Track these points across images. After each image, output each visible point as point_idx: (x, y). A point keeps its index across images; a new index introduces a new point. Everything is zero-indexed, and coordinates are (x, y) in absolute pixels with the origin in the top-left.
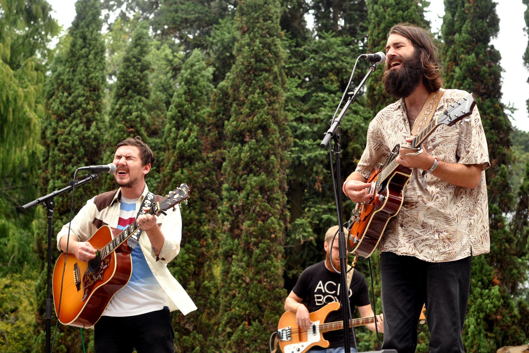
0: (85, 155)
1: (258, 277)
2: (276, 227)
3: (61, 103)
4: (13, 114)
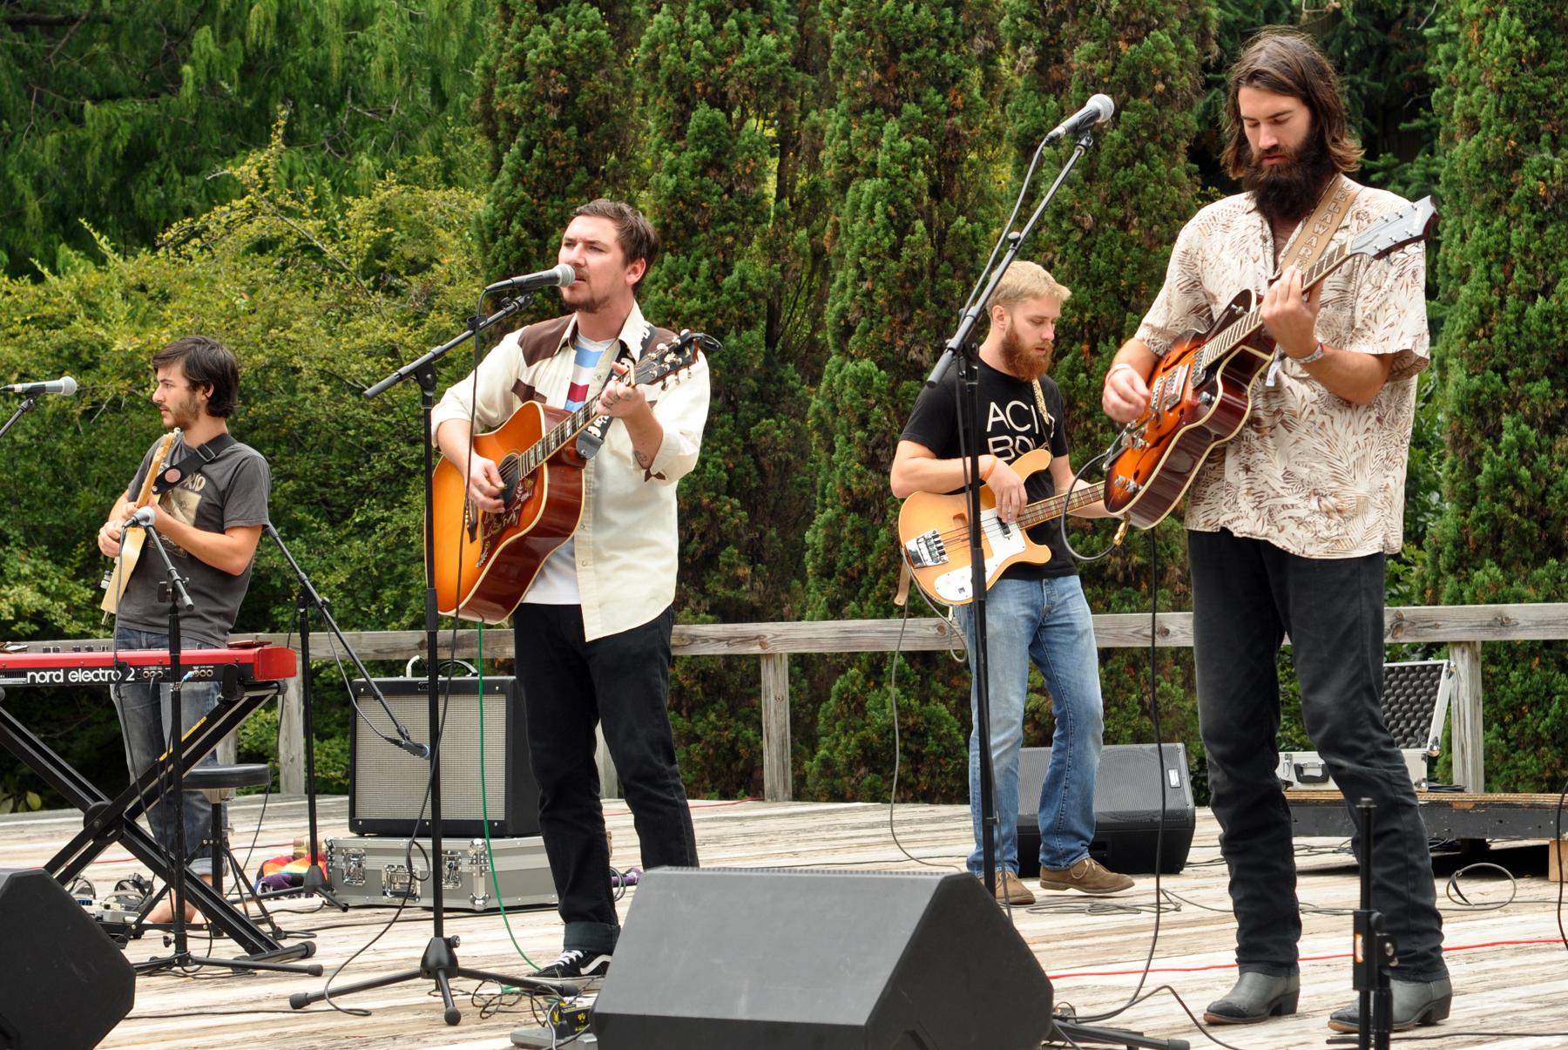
1: (1117, 212)
2: (1168, 61)
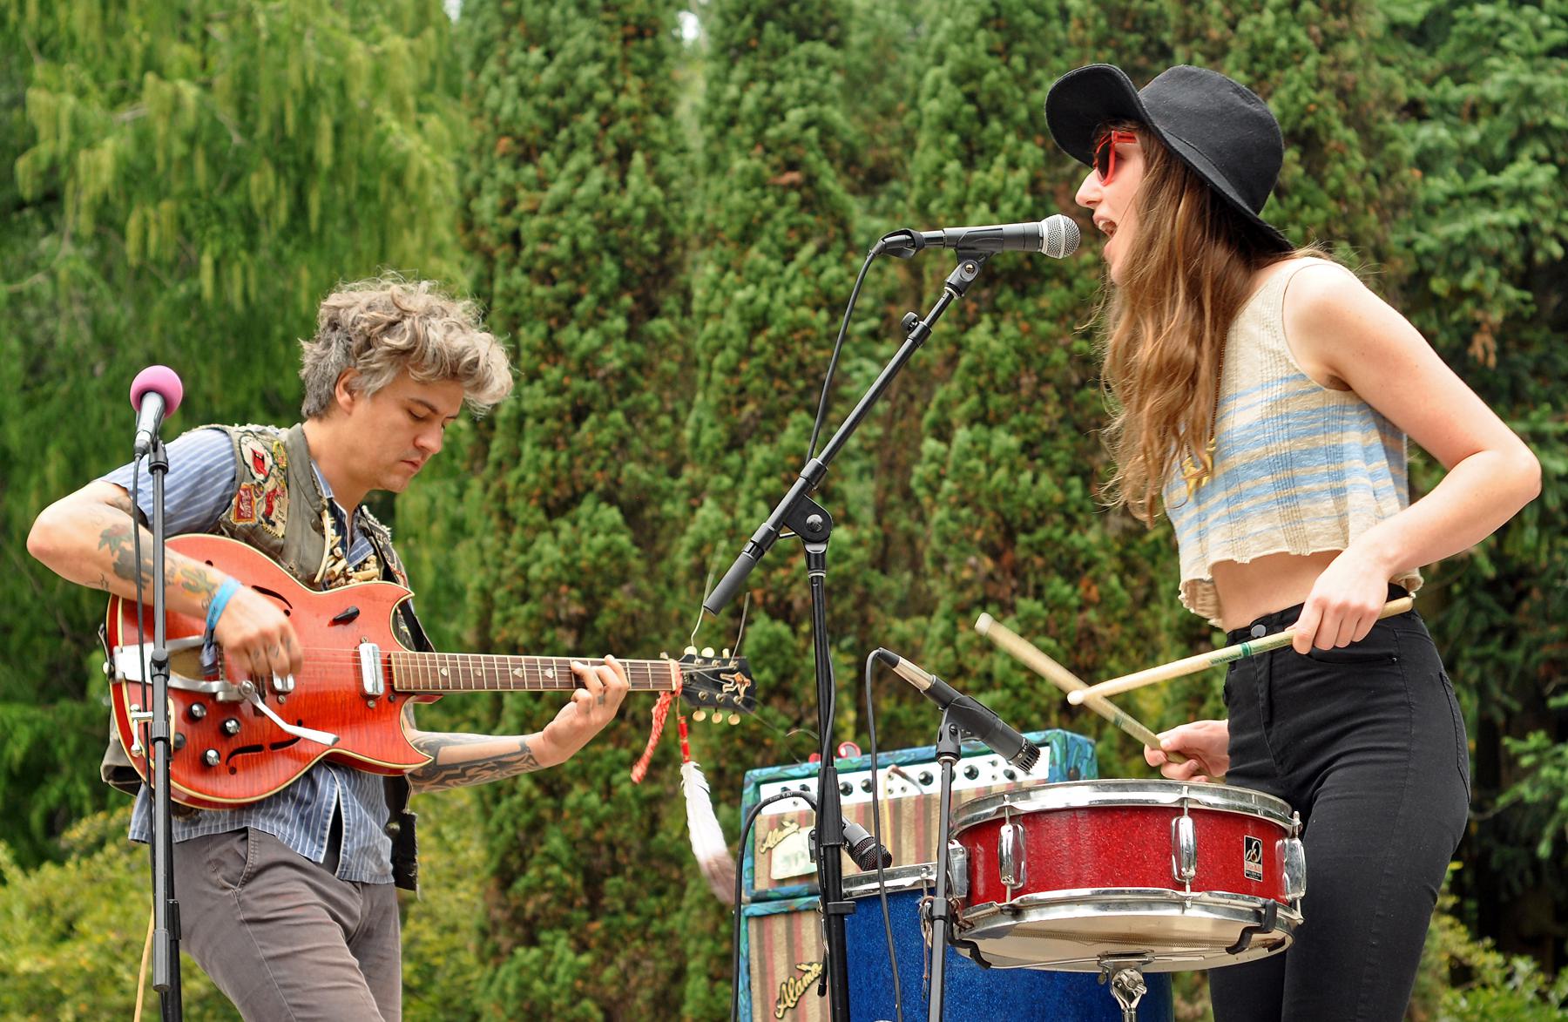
0: (624, 285)
3: (524, 92)
4: (338, 145)
